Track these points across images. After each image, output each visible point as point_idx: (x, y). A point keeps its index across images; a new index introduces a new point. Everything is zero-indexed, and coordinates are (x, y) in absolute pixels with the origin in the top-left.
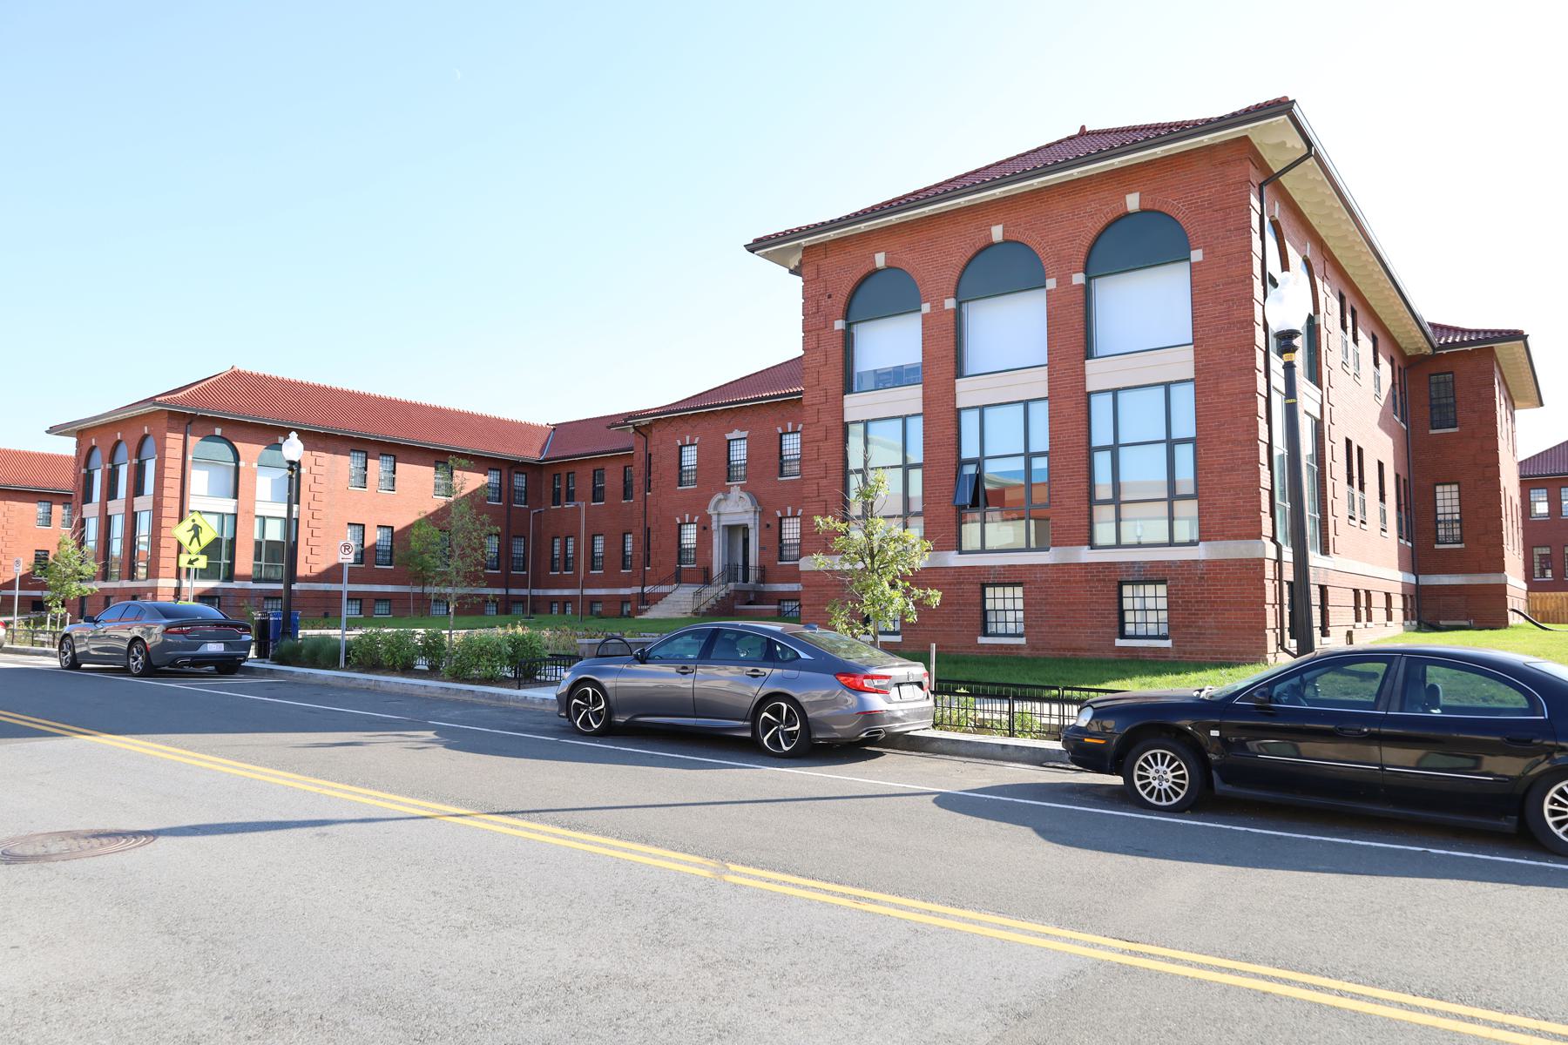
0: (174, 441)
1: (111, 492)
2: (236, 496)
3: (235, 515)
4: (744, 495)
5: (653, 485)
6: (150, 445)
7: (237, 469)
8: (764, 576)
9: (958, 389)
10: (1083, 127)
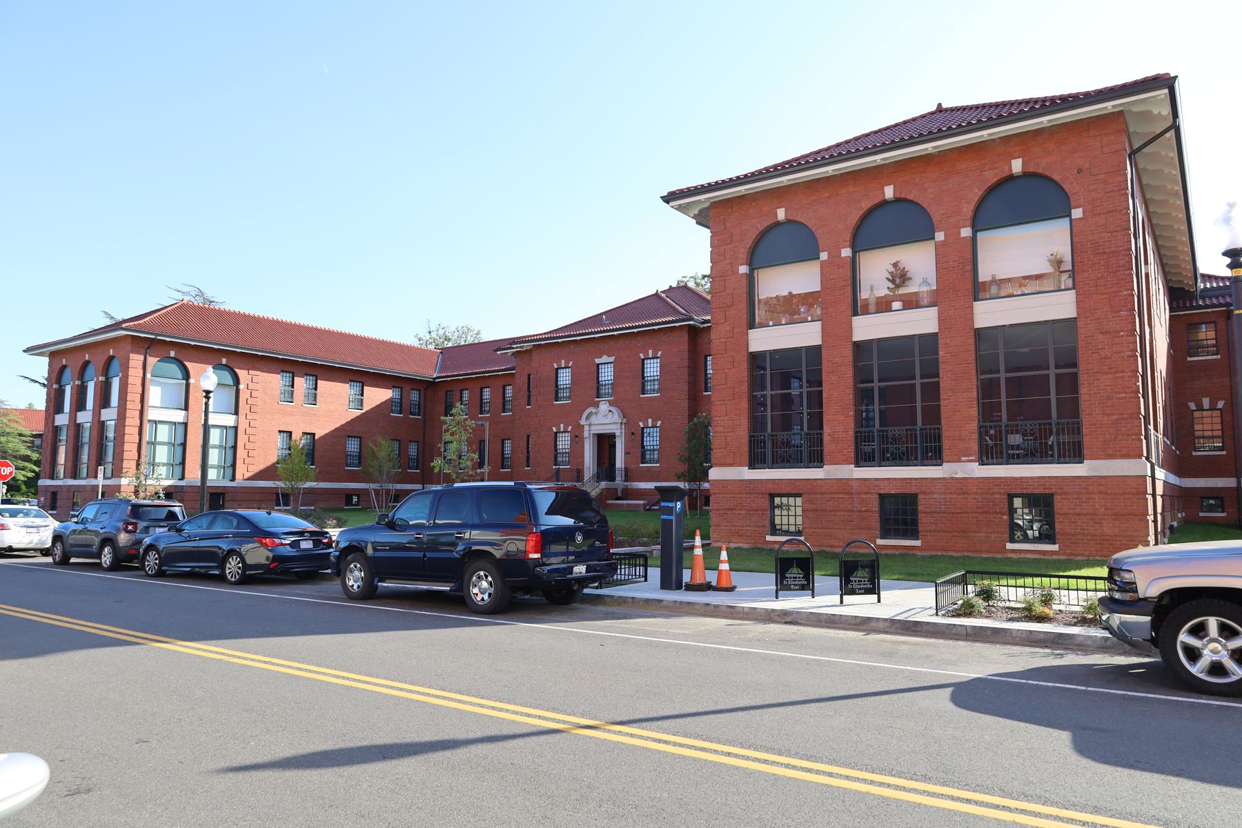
0: (136, 360)
1: (80, 404)
2: (186, 408)
3: (186, 424)
4: (612, 409)
5: (532, 399)
6: (115, 365)
7: (188, 385)
8: (628, 476)
9: (854, 325)
10: (940, 105)
